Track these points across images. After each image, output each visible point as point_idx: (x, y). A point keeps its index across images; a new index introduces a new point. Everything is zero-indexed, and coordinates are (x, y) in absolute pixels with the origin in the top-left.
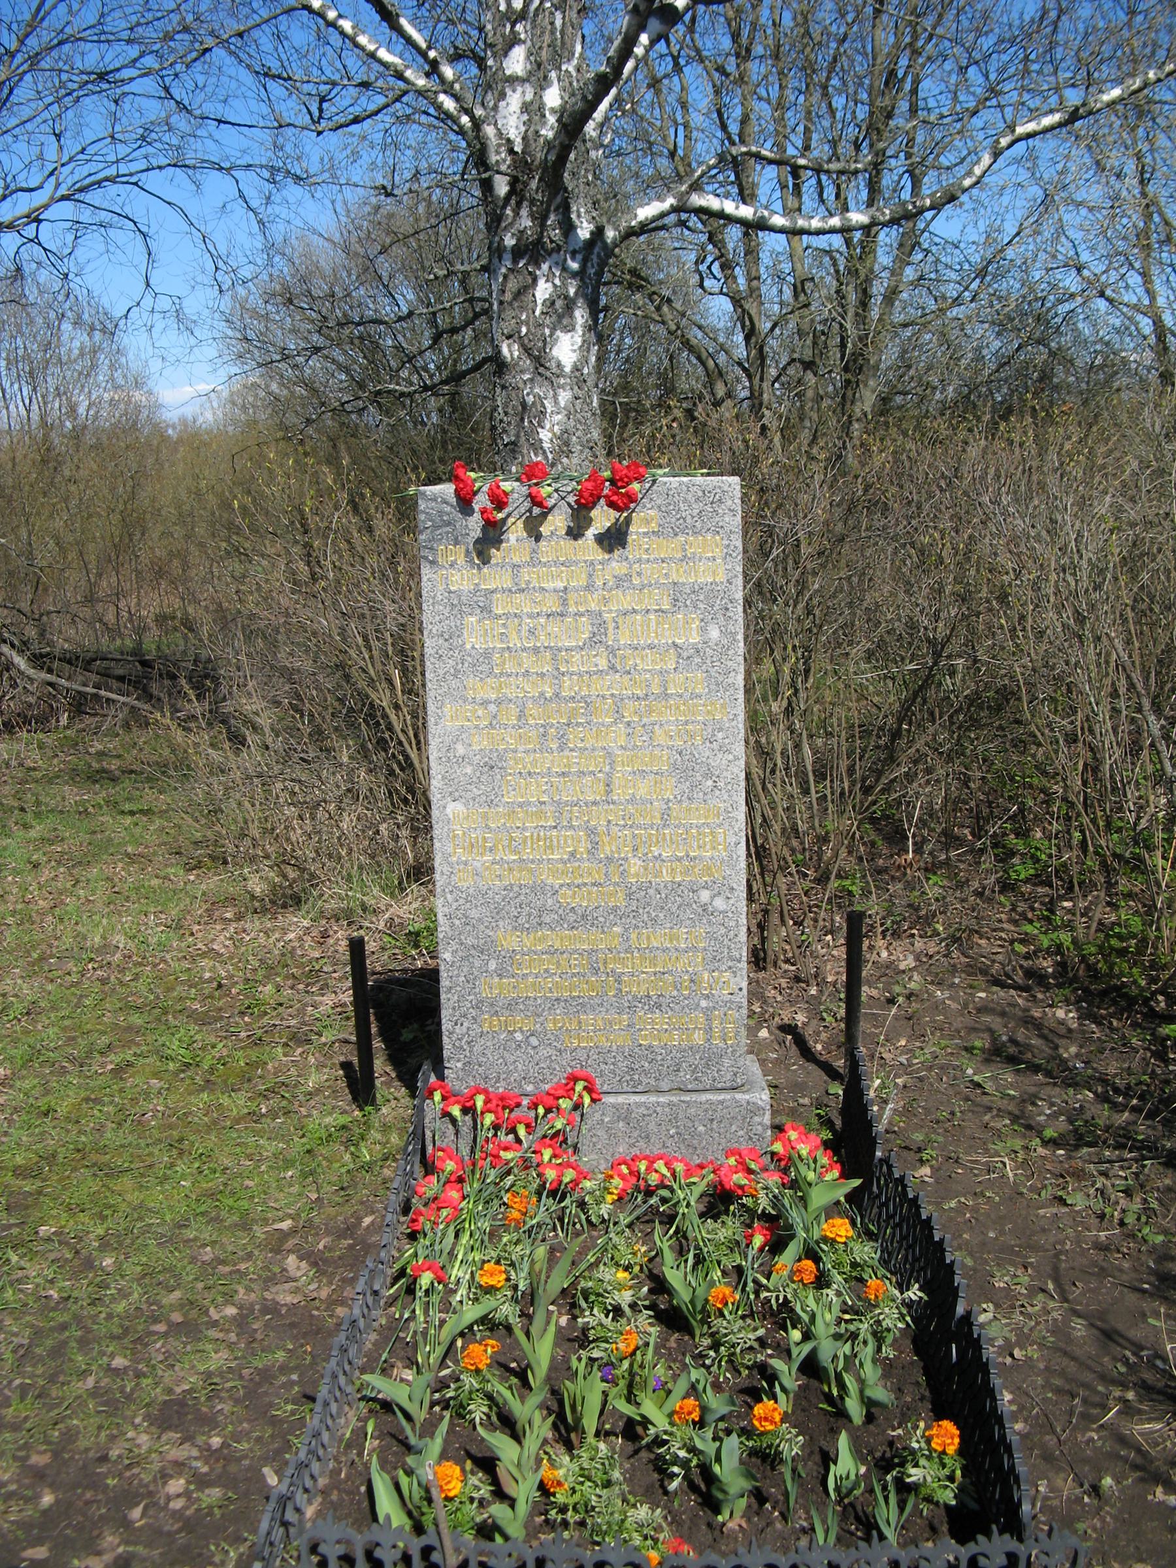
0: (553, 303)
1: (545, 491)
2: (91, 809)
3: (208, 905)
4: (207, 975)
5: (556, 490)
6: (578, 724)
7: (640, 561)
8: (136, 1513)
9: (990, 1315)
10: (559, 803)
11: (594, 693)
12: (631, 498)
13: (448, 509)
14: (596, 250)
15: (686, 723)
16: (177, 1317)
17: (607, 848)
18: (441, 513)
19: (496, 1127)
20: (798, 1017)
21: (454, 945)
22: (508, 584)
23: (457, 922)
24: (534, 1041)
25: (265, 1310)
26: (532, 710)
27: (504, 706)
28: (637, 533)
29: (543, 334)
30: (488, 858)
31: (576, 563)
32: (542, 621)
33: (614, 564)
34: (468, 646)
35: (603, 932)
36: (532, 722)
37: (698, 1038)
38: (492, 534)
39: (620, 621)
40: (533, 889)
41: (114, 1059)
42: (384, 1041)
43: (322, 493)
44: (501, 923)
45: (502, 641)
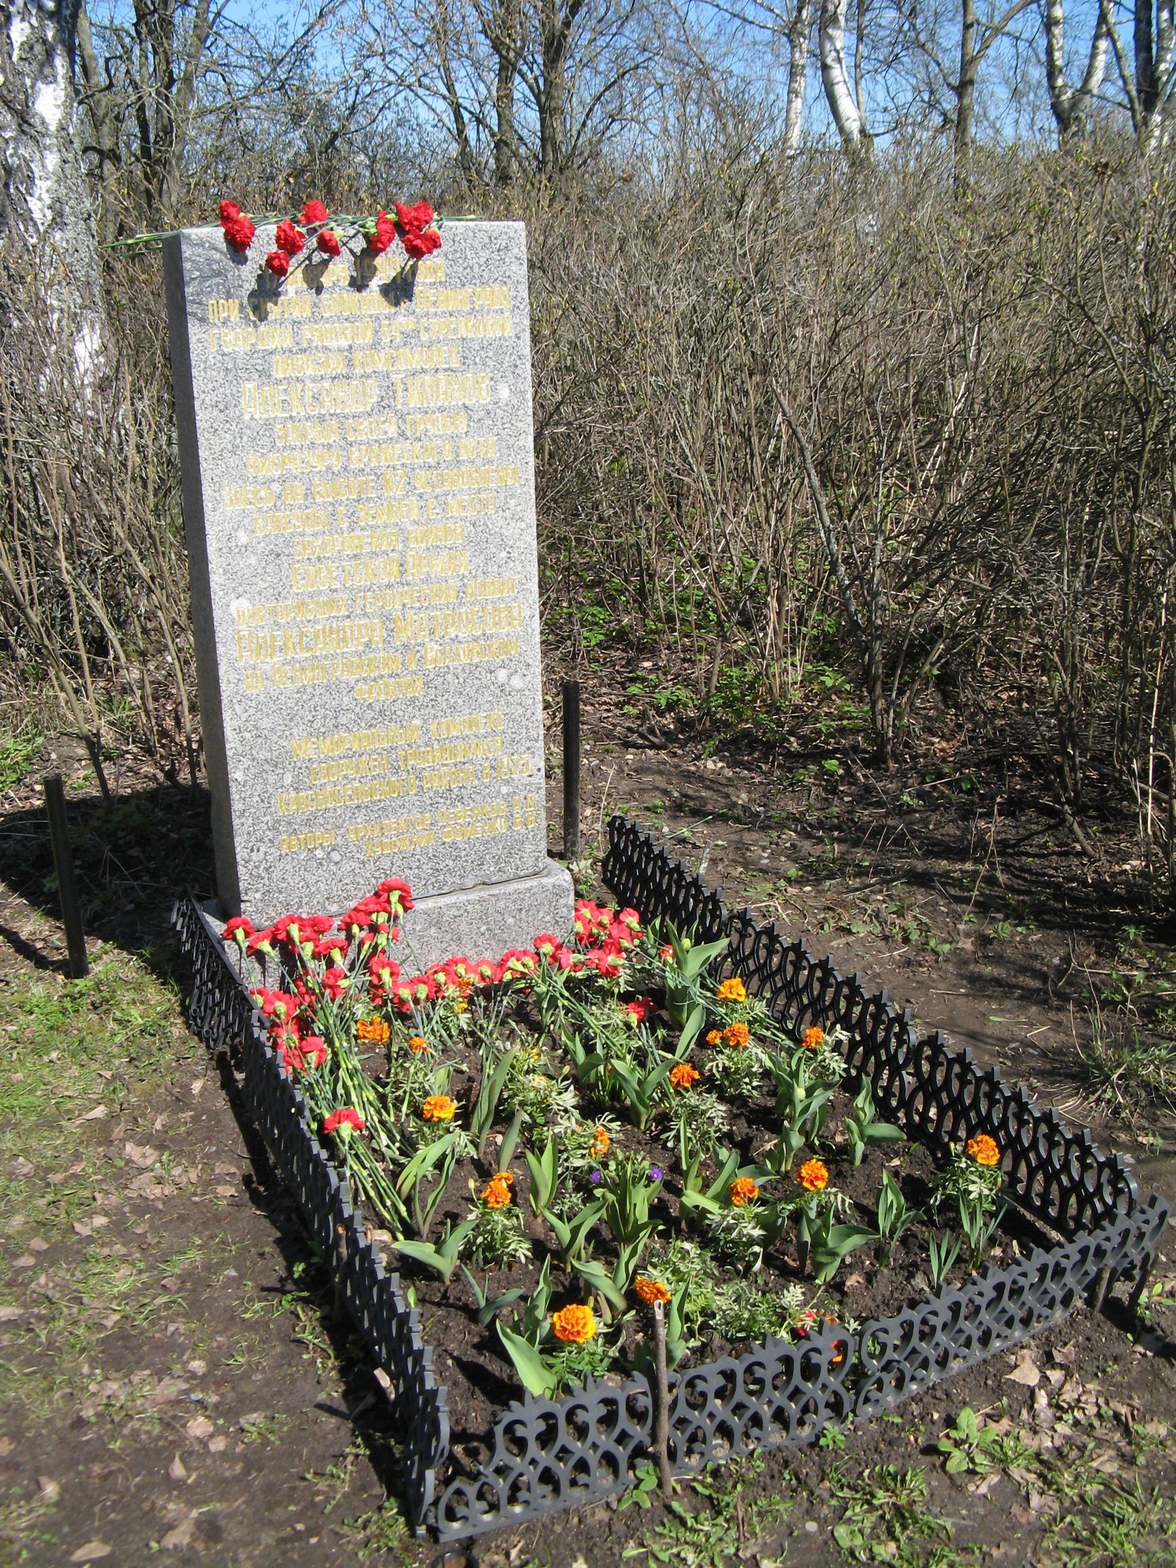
0: (31, 48)
7: (427, 314)
13: (217, 256)
15: (479, 491)
21: (246, 762)
22: (288, 343)
23: (248, 735)
24: (336, 856)
26: (320, 486)
27: (288, 484)
28: (424, 284)
29: (23, 85)
31: (360, 318)
32: (327, 384)
33: (401, 319)
34: (247, 417)
37: (500, 826)
39: (409, 382)
40: (328, 689)
44: (295, 731)
45: (284, 410)
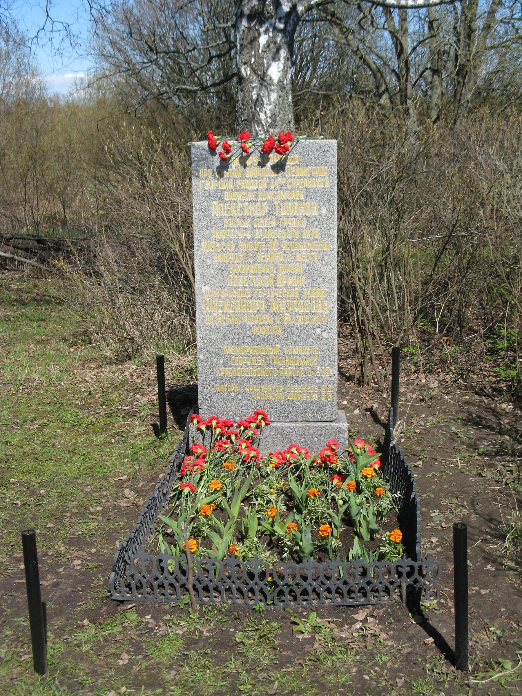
0: (268, 46)
1: (248, 145)
2: (12, 319)
3: (82, 362)
4: (83, 389)
5: (254, 145)
6: (262, 252)
7: (291, 177)
8: (61, 570)
9: (436, 514)
10: (253, 287)
11: (269, 237)
12: (286, 149)
14: (292, 17)
16: (75, 511)
17: (275, 308)
18: (201, 154)
19: (222, 435)
20: (374, 405)
22: (231, 187)
23: (206, 341)
24: (240, 397)
25: (114, 509)
26: (241, 245)
27: (228, 243)
28: (290, 165)
30: (220, 312)
32: (246, 204)
33: (279, 179)
35: (272, 347)
36: (241, 250)
37: (315, 397)
38: (225, 164)
40: (240, 326)
41: (39, 422)
42: (174, 415)
43: (150, 145)
44: (226, 342)
45: (228, 213)
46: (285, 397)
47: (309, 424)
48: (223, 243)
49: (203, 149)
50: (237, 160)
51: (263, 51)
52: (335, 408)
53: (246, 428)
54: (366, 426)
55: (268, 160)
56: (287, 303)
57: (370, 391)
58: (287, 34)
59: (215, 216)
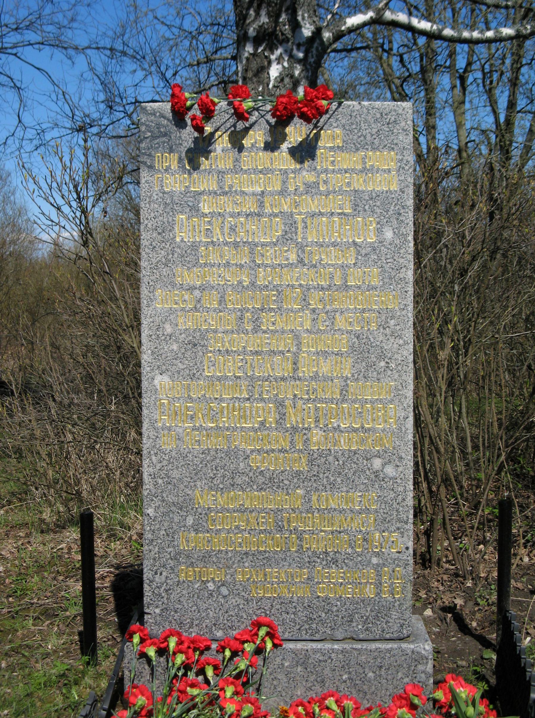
0: (282, 80)
10: (252, 378)
14: (315, 45)
17: (293, 419)
18: (158, 126)
19: (187, 667)
22: (214, 187)
23: (160, 481)
24: (224, 591)
26: (231, 295)
28: (325, 148)
33: (304, 173)
35: (288, 494)
37: (370, 592)
38: (202, 147)
44: (199, 483)
45: (207, 236)
46: (313, 592)
47: (359, 646)
48: (197, 293)
49: (162, 116)
50: (226, 137)
51: (274, 86)
52: (408, 614)
53: (234, 654)
54: (448, 639)
55: (284, 137)
56: (317, 409)
57: (445, 577)
58: (308, 67)
59: (182, 241)
